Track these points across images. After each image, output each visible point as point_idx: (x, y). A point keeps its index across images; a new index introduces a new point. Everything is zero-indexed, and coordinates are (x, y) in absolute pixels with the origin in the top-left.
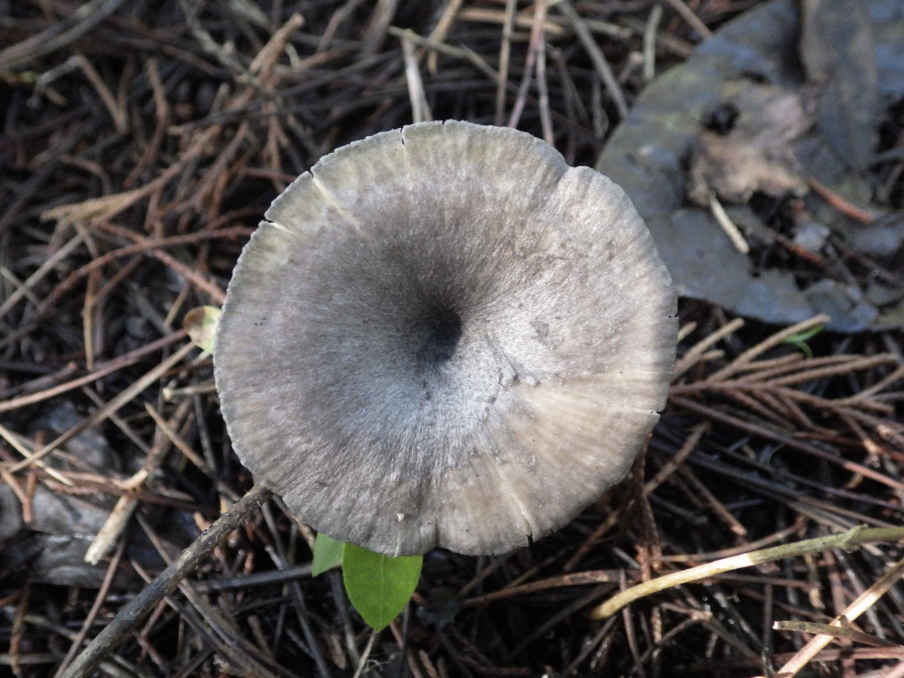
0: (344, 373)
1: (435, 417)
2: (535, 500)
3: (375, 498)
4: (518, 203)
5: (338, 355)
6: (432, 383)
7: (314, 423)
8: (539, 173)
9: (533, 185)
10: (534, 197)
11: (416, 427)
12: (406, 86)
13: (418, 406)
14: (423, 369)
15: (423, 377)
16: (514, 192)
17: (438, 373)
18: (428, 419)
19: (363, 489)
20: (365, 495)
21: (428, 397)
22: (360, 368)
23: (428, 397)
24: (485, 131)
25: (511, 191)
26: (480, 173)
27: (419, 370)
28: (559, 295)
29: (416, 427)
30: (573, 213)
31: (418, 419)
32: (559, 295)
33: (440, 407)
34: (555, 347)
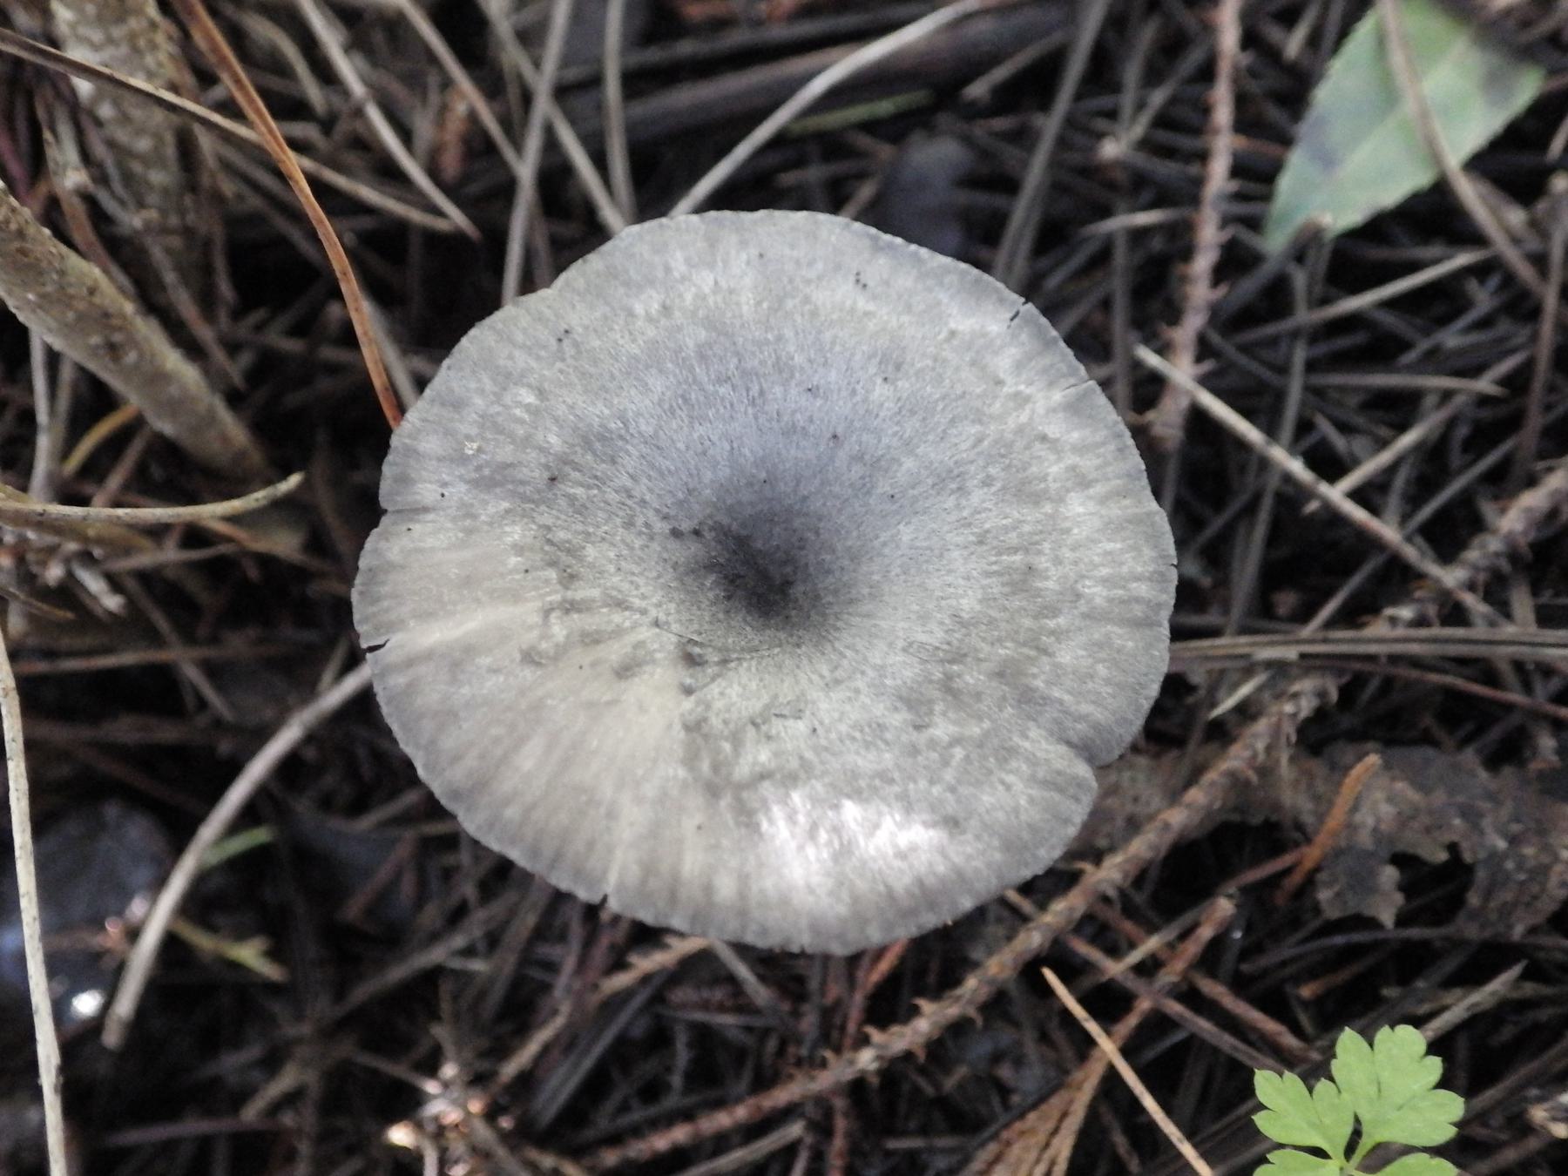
0: (755, 390)
1: (640, 533)
2: (457, 660)
3: (518, 412)
4: (1035, 670)
5: (785, 384)
6: (694, 549)
7: (680, 329)
8: (1086, 708)
9: (1066, 697)
10: (1046, 700)
11: (630, 497)
12: (1142, 941)
13: (666, 510)
14: (720, 542)
15: (708, 535)
16: (1057, 666)
17: (710, 567)
18: (640, 521)
19: (541, 393)
20: (530, 398)
21: (676, 533)
22: (756, 418)
23: (676, 533)
24: (1160, 625)
25: (1059, 659)
26: (1085, 616)
27: (723, 533)
28: (858, 735)
29: (630, 497)
30: (1014, 764)
31: (643, 503)
32: (858, 735)
33: (655, 546)
34: (754, 724)
